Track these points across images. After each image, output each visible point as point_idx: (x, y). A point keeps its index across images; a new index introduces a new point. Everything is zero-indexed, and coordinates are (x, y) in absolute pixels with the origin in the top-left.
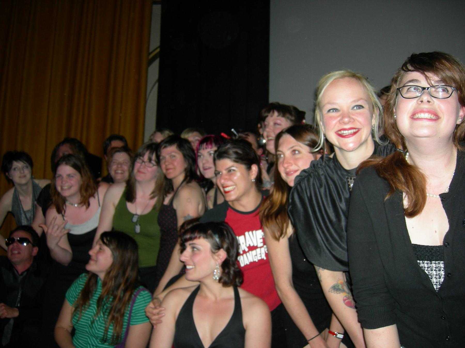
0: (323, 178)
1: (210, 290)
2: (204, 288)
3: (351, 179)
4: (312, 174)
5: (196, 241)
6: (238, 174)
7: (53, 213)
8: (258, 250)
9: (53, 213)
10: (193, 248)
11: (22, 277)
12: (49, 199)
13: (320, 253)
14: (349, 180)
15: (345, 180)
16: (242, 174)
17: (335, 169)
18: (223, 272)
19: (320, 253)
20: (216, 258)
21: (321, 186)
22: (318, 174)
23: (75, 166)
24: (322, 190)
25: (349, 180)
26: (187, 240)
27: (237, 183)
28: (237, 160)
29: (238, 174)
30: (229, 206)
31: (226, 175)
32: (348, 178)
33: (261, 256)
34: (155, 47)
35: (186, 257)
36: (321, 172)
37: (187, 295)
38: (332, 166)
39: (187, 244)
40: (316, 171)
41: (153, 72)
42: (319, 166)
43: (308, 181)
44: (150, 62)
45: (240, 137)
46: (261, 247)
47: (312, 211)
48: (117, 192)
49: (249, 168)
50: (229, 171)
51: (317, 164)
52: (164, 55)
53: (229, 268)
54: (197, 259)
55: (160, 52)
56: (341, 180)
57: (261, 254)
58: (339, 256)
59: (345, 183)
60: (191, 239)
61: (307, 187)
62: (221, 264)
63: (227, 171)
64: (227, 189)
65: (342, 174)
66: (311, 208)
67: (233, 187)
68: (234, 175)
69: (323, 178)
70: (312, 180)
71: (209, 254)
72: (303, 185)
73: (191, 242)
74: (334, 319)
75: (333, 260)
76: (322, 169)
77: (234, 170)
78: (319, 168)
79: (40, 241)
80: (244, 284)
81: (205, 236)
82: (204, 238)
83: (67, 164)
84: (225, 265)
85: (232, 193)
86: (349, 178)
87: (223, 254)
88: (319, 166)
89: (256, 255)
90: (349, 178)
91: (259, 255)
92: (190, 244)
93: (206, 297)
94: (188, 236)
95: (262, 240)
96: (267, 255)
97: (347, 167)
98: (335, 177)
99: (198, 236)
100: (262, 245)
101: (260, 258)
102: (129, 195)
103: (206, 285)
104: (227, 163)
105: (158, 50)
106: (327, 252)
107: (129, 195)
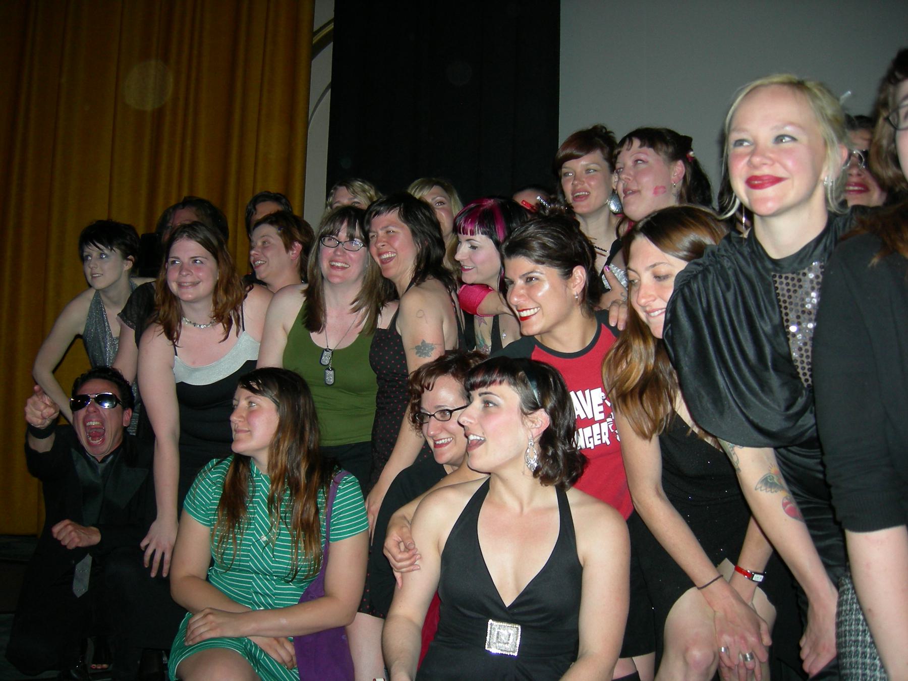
0: (730, 272)
1: (512, 491)
2: (498, 487)
3: (780, 277)
4: (711, 268)
5: (492, 389)
6: (546, 287)
7: (156, 341)
8: (596, 427)
9: (156, 341)
10: (487, 403)
11: (103, 465)
12: (153, 309)
13: (722, 413)
14: (777, 279)
15: (770, 279)
16: (552, 286)
17: (751, 258)
18: (543, 456)
19: (722, 413)
20: (530, 424)
21: (728, 287)
22: (722, 267)
23: (206, 244)
24: (730, 296)
25: (777, 279)
26: (474, 387)
27: (546, 303)
28: (541, 259)
29: (546, 287)
30: (537, 342)
31: (522, 288)
32: (774, 276)
33: (601, 439)
34: (326, 21)
35: (470, 417)
36: (726, 264)
37: (465, 501)
38: (746, 253)
39: (475, 394)
40: (717, 262)
41: (322, 68)
42: (723, 253)
43: (705, 279)
44: (315, 50)
45: (552, 211)
46: (600, 422)
47: (710, 334)
48: (292, 305)
49: (568, 274)
50: (529, 280)
51: (719, 250)
52: (340, 36)
53: (555, 447)
54: (493, 424)
55: (334, 30)
56: (762, 278)
57: (600, 434)
58: (756, 421)
59: (769, 285)
60: (483, 384)
61: (702, 289)
62: (537, 439)
63: (525, 278)
64: (524, 314)
65: (764, 267)
66: (708, 327)
67: (536, 310)
68: (538, 288)
69: (730, 272)
70: (710, 277)
71: (516, 417)
72: (695, 286)
73: (483, 390)
74: (752, 525)
75: (746, 424)
76: (729, 257)
77: (537, 279)
78: (723, 256)
79: (129, 396)
80: (579, 483)
81: (512, 380)
82: (510, 384)
83: (190, 237)
84: (547, 439)
85: (534, 319)
86: (778, 275)
87: (542, 419)
88: (723, 253)
89: (592, 437)
90: (778, 275)
91: (596, 437)
92: (480, 395)
93: (502, 506)
94: (479, 379)
95: (601, 408)
96: (612, 436)
97: (774, 254)
98: (751, 271)
99: (498, 380)
100: (602, 416)
101: (598, 443)
102: (312, 317)
103: (503, 480)
104: (521, 265)
105: (331, 26)
106: (737, 410)
107: (312, 317)
